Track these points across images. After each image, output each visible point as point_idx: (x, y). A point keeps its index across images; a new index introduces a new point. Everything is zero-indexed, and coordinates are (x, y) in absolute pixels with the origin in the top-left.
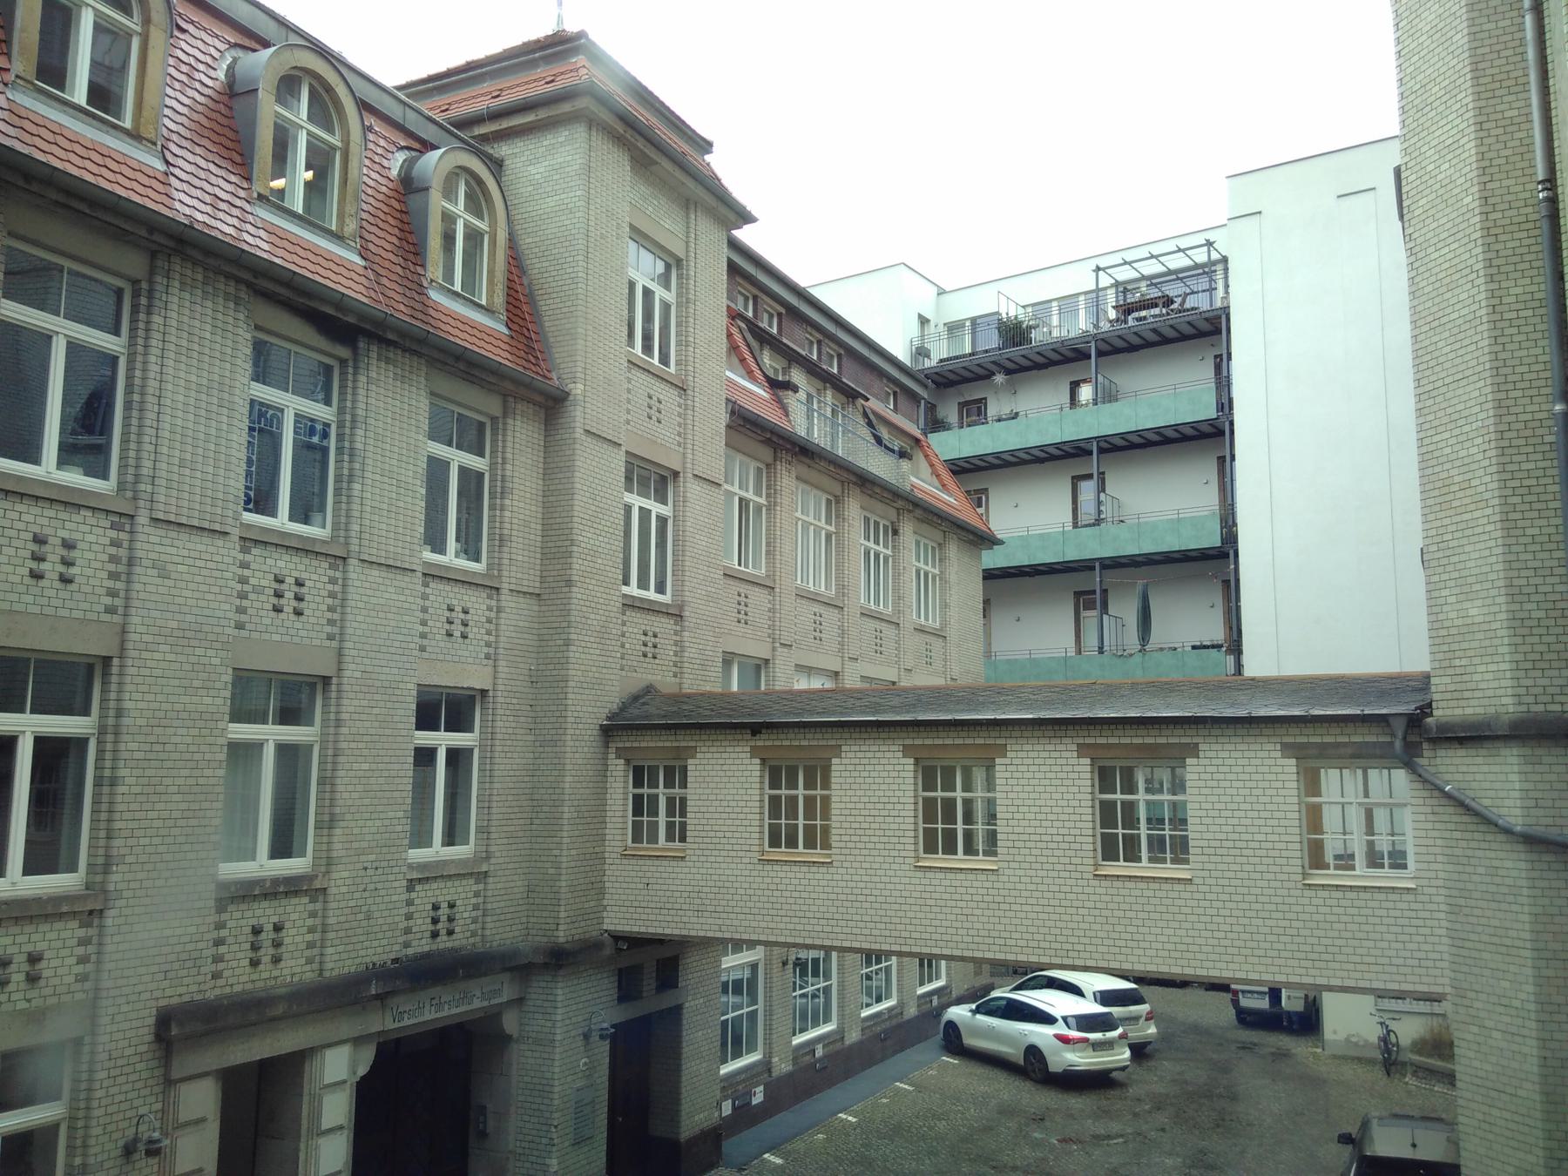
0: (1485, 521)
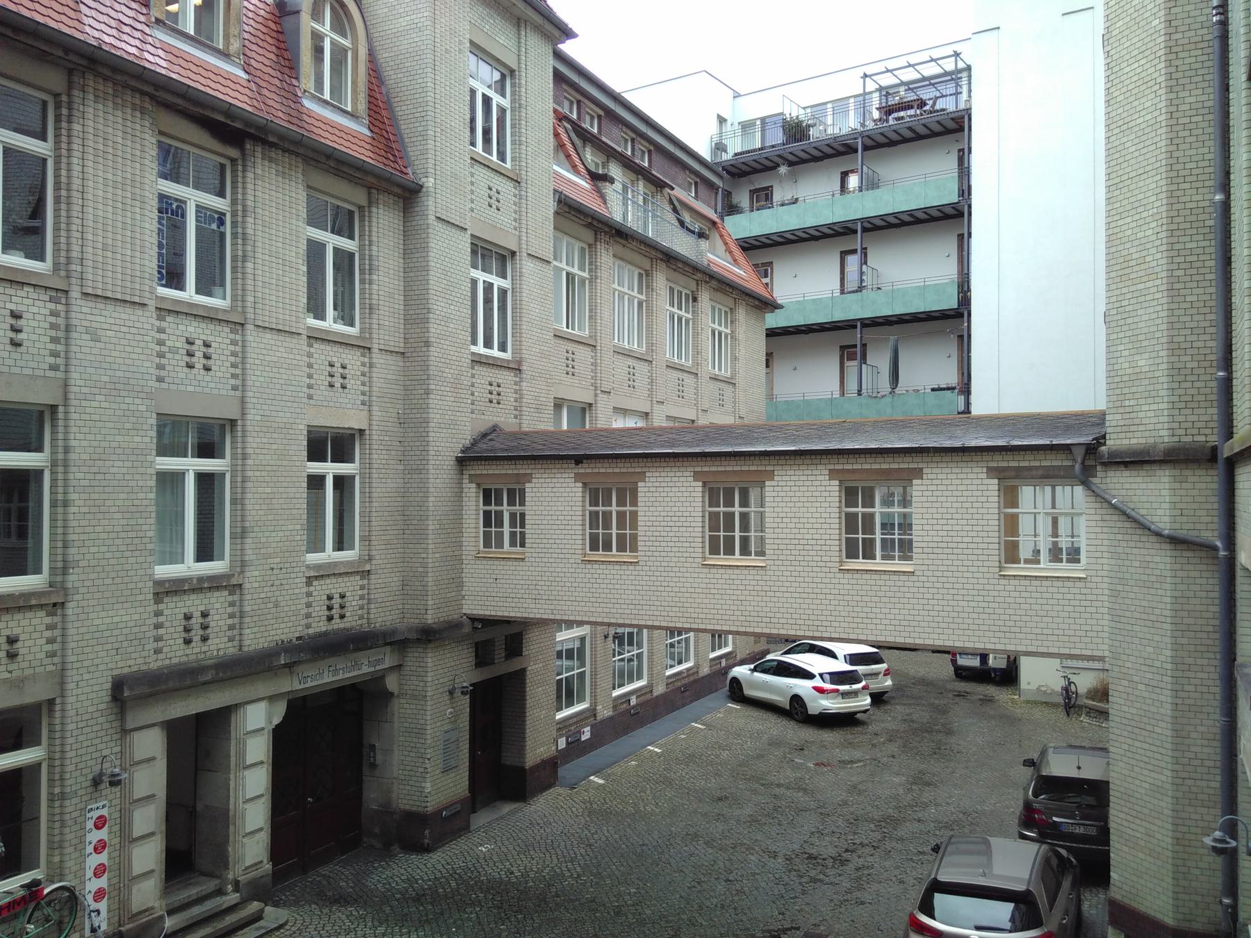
0: (1156, 289)
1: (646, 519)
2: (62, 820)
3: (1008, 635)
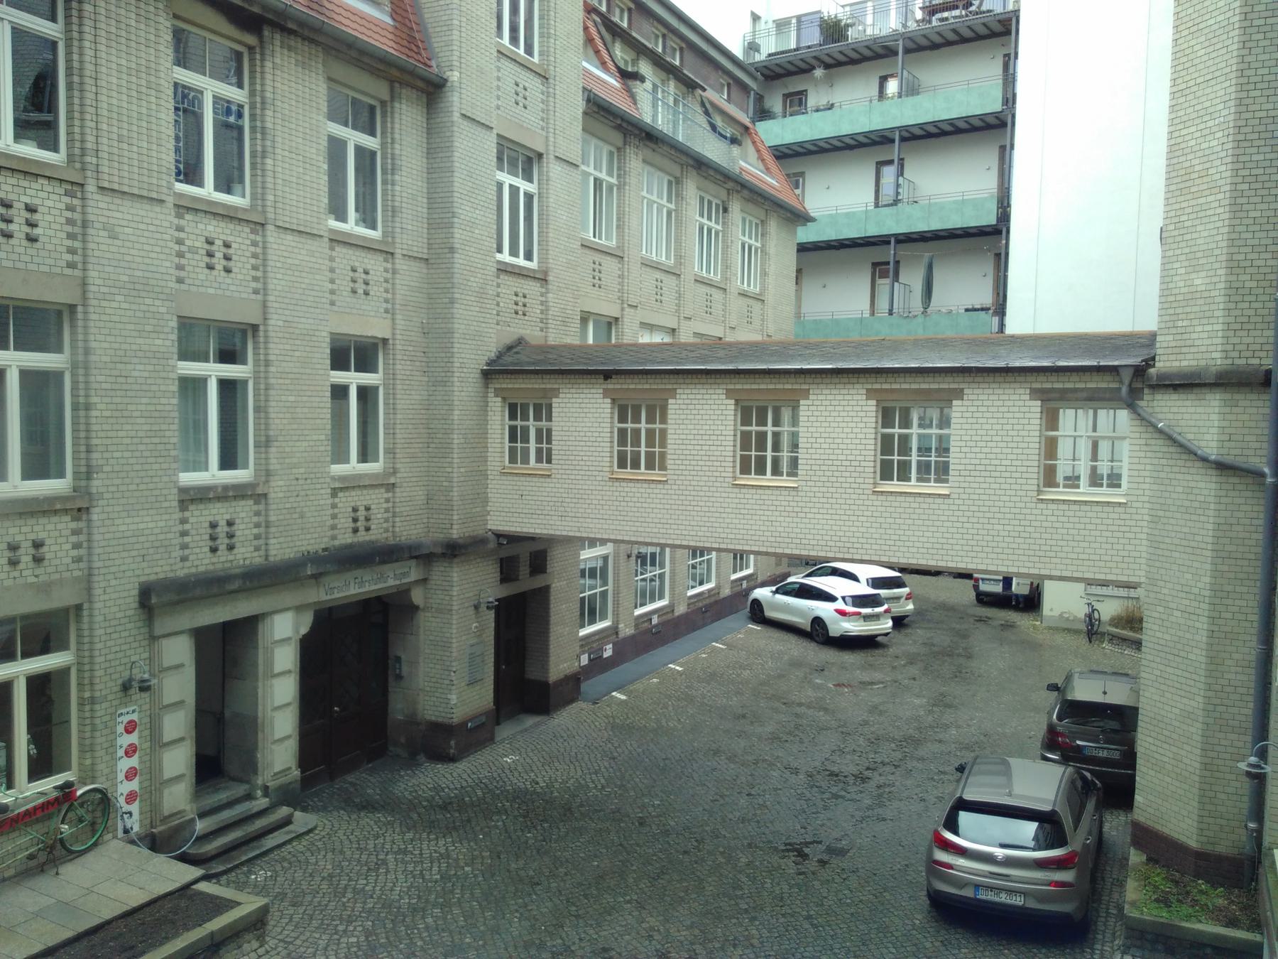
1: (676, 437)
2: (93, 724)
3: (1043, 559)
